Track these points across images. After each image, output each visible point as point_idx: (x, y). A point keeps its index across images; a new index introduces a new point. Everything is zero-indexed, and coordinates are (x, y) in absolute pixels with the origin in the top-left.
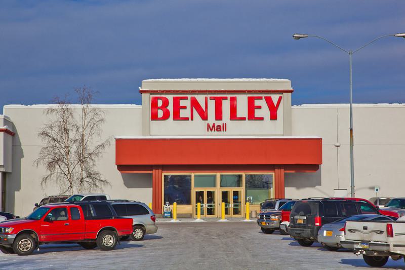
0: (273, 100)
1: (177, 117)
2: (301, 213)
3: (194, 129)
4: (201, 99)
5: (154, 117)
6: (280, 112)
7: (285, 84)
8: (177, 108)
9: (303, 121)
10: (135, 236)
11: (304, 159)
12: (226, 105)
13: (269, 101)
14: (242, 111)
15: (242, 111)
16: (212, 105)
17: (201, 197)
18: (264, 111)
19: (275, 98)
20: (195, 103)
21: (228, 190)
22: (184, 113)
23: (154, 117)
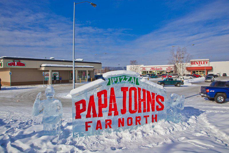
0: (96, 109)
1: (194, 64)
2: (219, 98)
3: (196, 66)
4: (197, 62)
5: (192, 64)
6: (208, 63)
7: (208, 60)
8: (194, 63)
9: (211, 64)
10: (193, 117)
11: (211, 69)
12: (201, 62)
13: (206, 62)
14: (203, 63)
15: (203, 63)
16: (199, 62)
17: (181, 82)
18: (206, 63)
19: (207, 61)
20: (197, 62)
21: (87, 119)
22: (195, 64)
23: (192, 64)
